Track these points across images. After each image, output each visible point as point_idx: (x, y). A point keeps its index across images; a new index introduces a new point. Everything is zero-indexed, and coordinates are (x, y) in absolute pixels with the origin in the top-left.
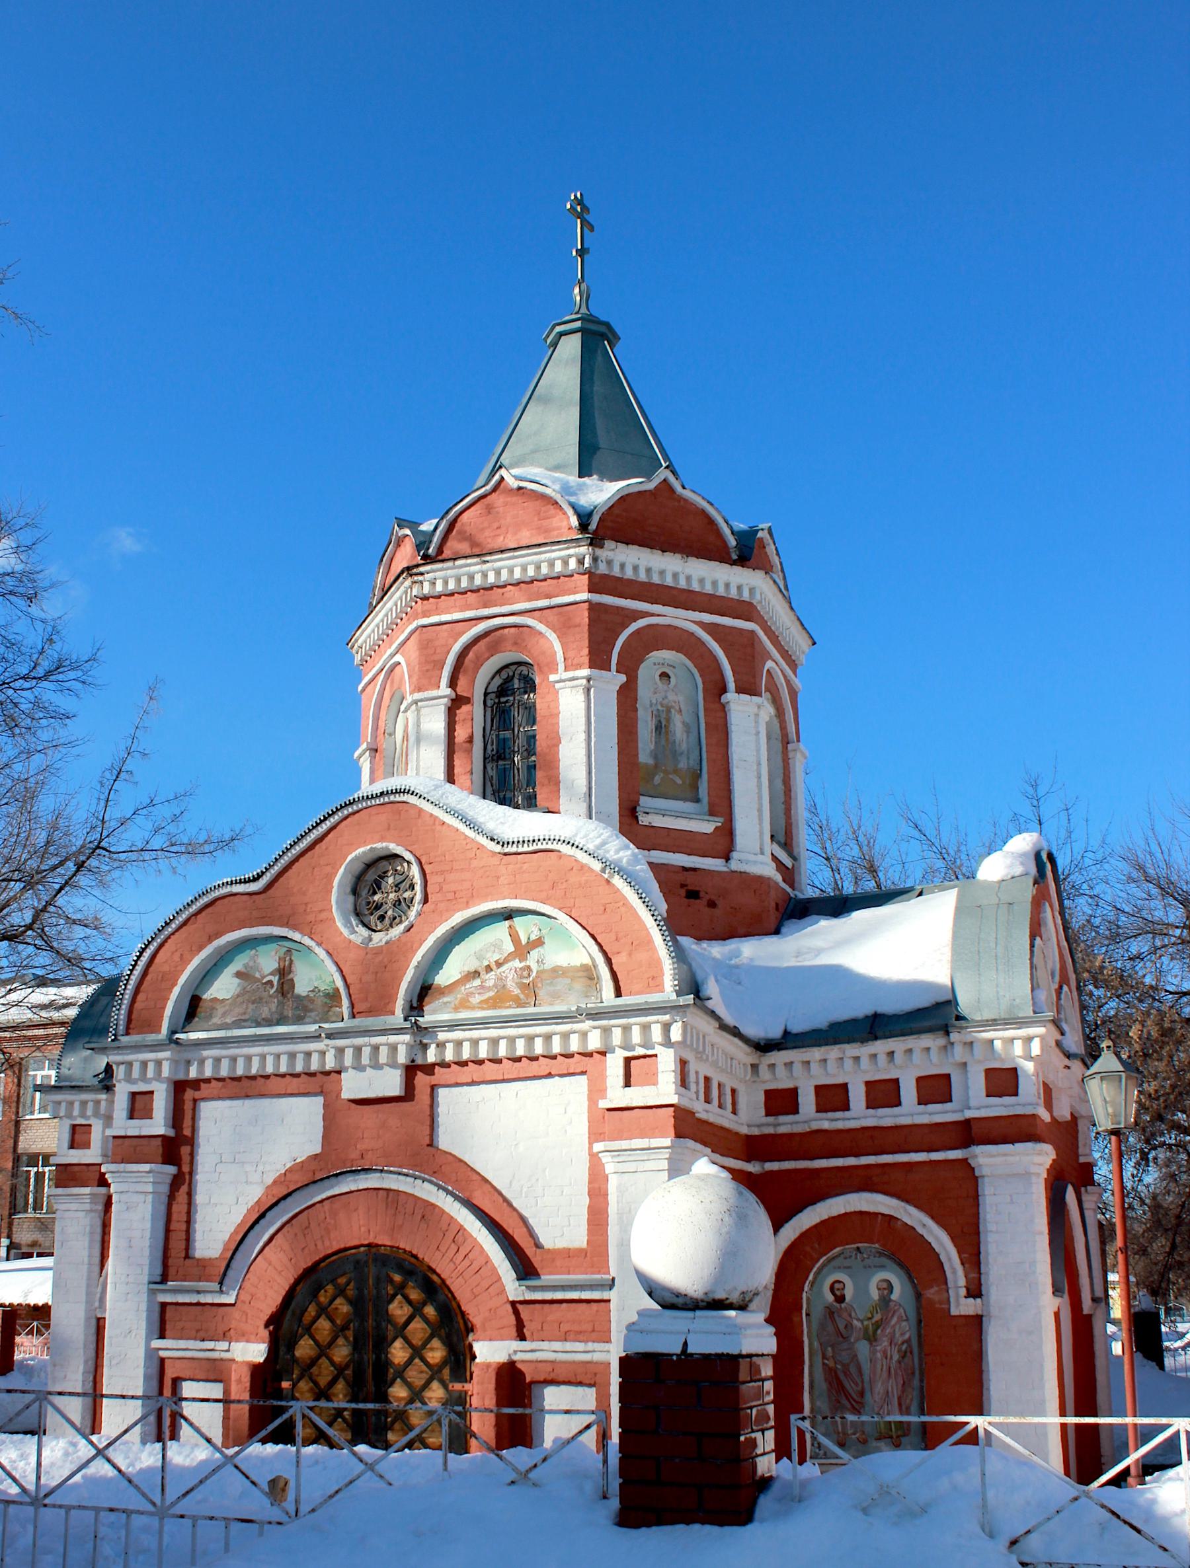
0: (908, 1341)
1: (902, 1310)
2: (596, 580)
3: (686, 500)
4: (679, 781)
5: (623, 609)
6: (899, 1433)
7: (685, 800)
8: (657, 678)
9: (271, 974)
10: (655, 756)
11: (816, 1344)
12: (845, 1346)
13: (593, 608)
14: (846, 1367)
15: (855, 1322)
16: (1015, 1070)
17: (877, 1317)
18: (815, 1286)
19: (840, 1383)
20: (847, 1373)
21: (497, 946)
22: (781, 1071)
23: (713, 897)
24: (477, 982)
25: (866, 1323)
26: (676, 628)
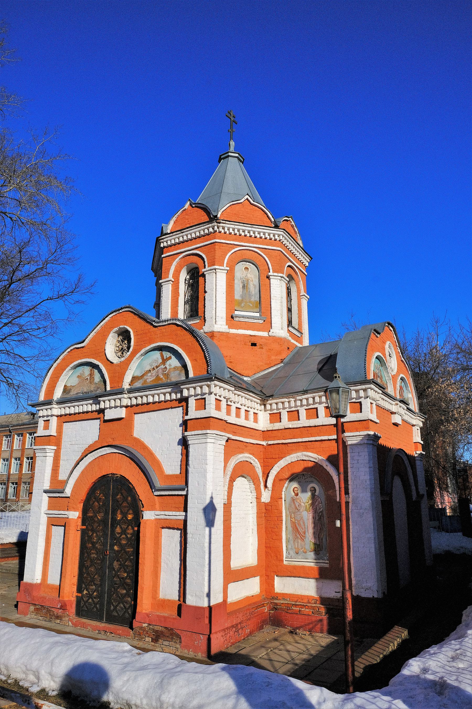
6: (319, 549)
9: (88, 376)
10: (242, 296)
11: (288, 512)
12: (298, 513)
20: (299, 524)
21: (157, 361)
22: (274, 406)
24: (149, 374)
25: (306, 504)
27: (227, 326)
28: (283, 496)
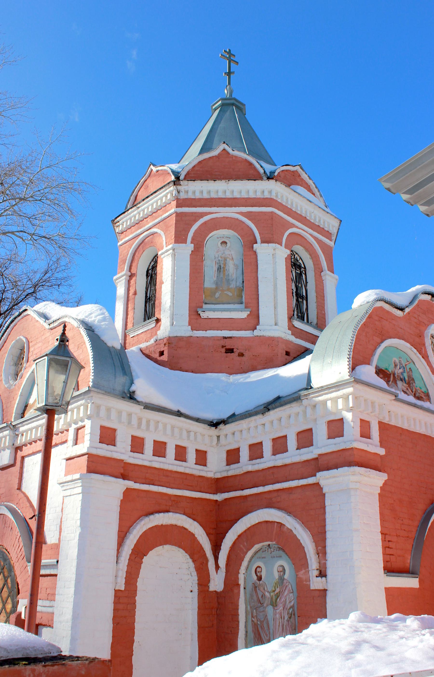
0: (292, 607)
1: (290, 586)
2: (181, 202)
3: (236, 157)
4: (230, 294)
5: (195, 213)
7: (234, 303)
8: (219, 244)
13: (178, 215)
14: (262, 622)
15: (267, 594)
16: (342, 420)
17: (278, 590)
18: (249, 570)
19: (259, 634)
20: (262, 627)
23: (242, 351)
26: (227, 218)
27: (190, 327)
28: (241, 582)
